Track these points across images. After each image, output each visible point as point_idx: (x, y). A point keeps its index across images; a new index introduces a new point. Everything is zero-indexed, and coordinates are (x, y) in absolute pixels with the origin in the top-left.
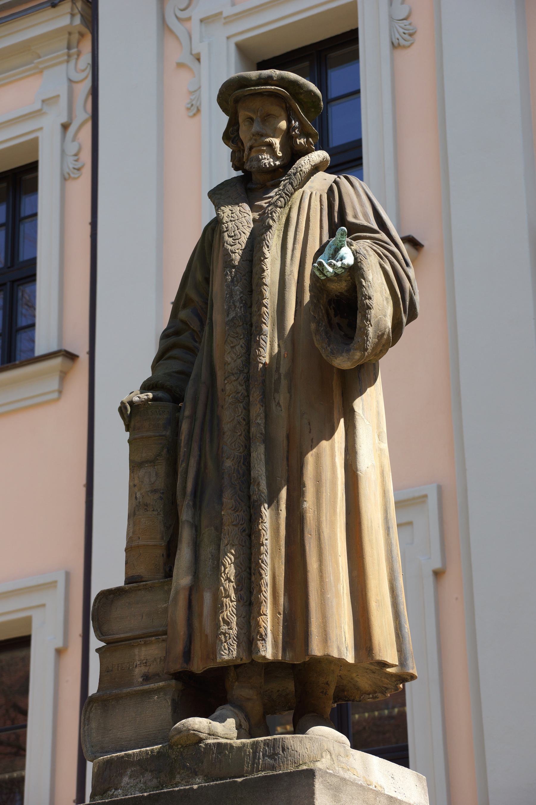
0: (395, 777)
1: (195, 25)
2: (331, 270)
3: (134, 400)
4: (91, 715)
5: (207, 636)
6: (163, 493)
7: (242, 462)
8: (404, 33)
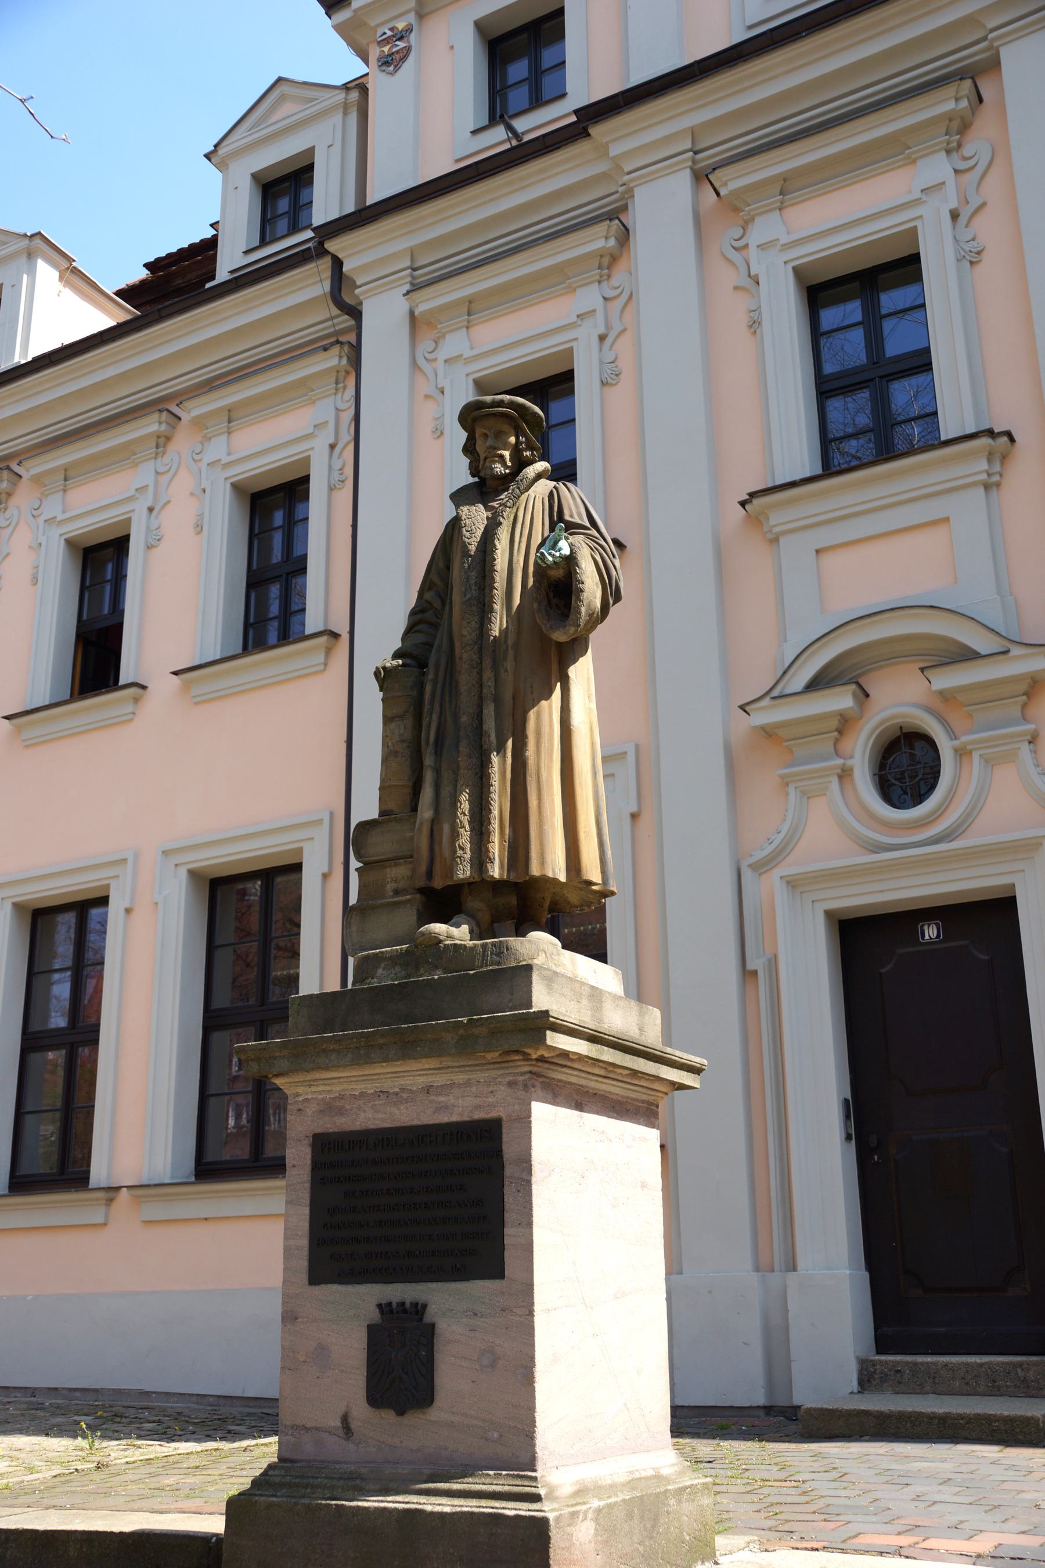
1: (440, 365)
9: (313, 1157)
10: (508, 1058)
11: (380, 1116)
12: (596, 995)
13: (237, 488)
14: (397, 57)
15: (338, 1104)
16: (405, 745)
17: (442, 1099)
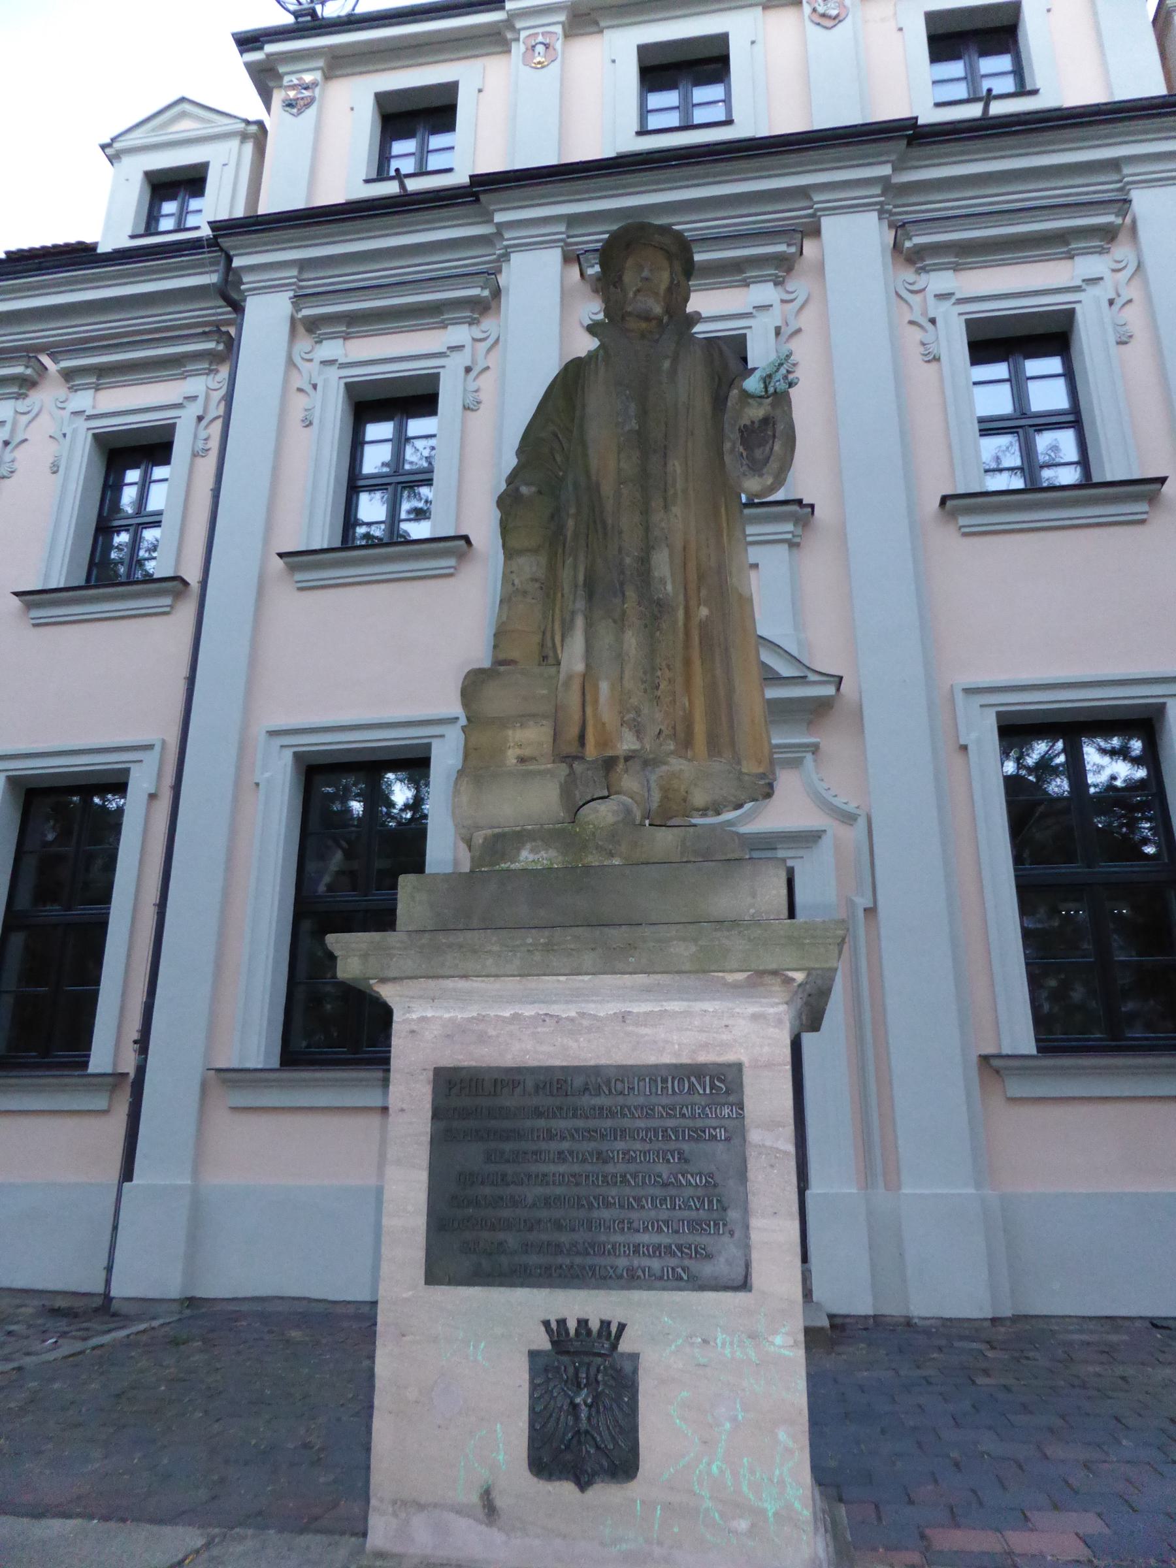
1: (315, 365)
9: (433, 1100)
11: (545, 1048)
14: (302, 103)
16: (537, 585)
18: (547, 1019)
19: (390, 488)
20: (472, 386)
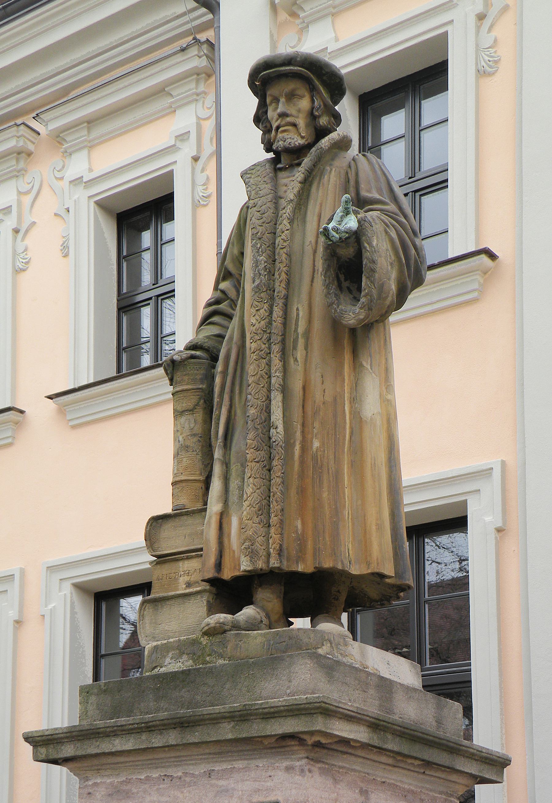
0: (390, 663)
2: (337, 236)
3: (174, 358)
4: (145, 613)
5: (234, 551)
6: (201, 437)
7: (264, 409)
8: (489, 61)
10: (284, 744)
12: (386, 687)
13: (103, 205)
15: (125, 788)
16: (195, 439)
17: (222, 783)
18: (165, 778)
19: (152, 302)
20: (487, 40)
